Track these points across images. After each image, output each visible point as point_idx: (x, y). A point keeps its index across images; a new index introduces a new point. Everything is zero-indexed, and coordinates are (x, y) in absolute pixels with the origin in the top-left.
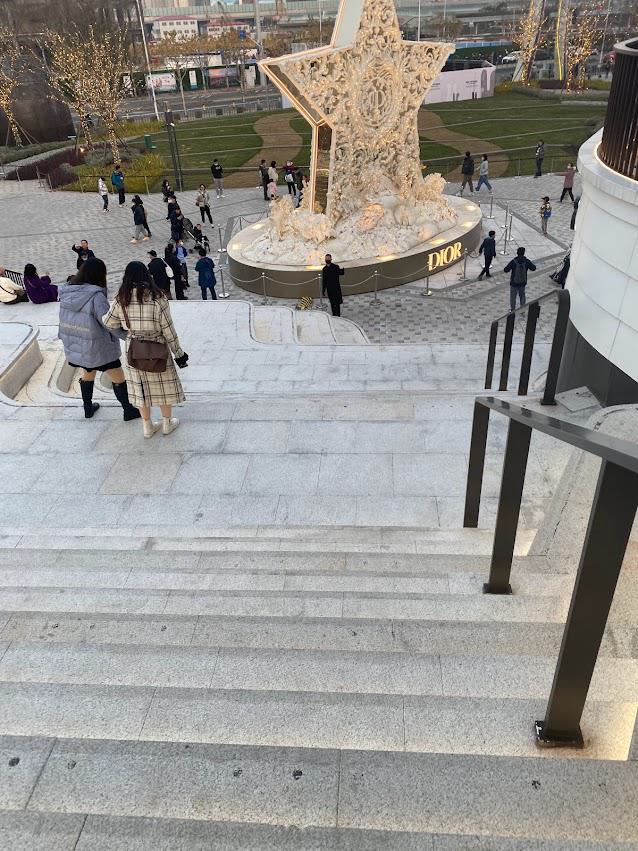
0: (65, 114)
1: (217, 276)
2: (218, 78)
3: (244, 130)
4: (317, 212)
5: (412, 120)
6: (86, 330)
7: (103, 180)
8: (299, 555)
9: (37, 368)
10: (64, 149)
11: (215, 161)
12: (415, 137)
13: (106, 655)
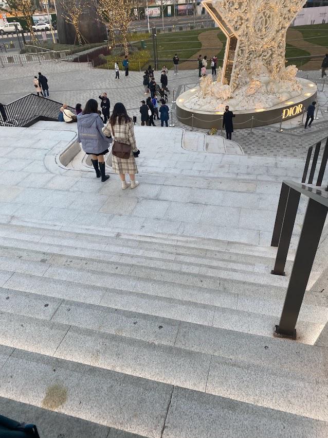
0: (103, 26)
1: (170, 115)
2: (182, 10)
3: (193, 39)
4: (225, 84)
5: (283, 35)
6: (95, 135)
7: (117, 63)
8: (185, 247)
9: (77, 154)
10: (102, 47)
11: (176, 55)
12: (284, 44)
13: (89, 274)
